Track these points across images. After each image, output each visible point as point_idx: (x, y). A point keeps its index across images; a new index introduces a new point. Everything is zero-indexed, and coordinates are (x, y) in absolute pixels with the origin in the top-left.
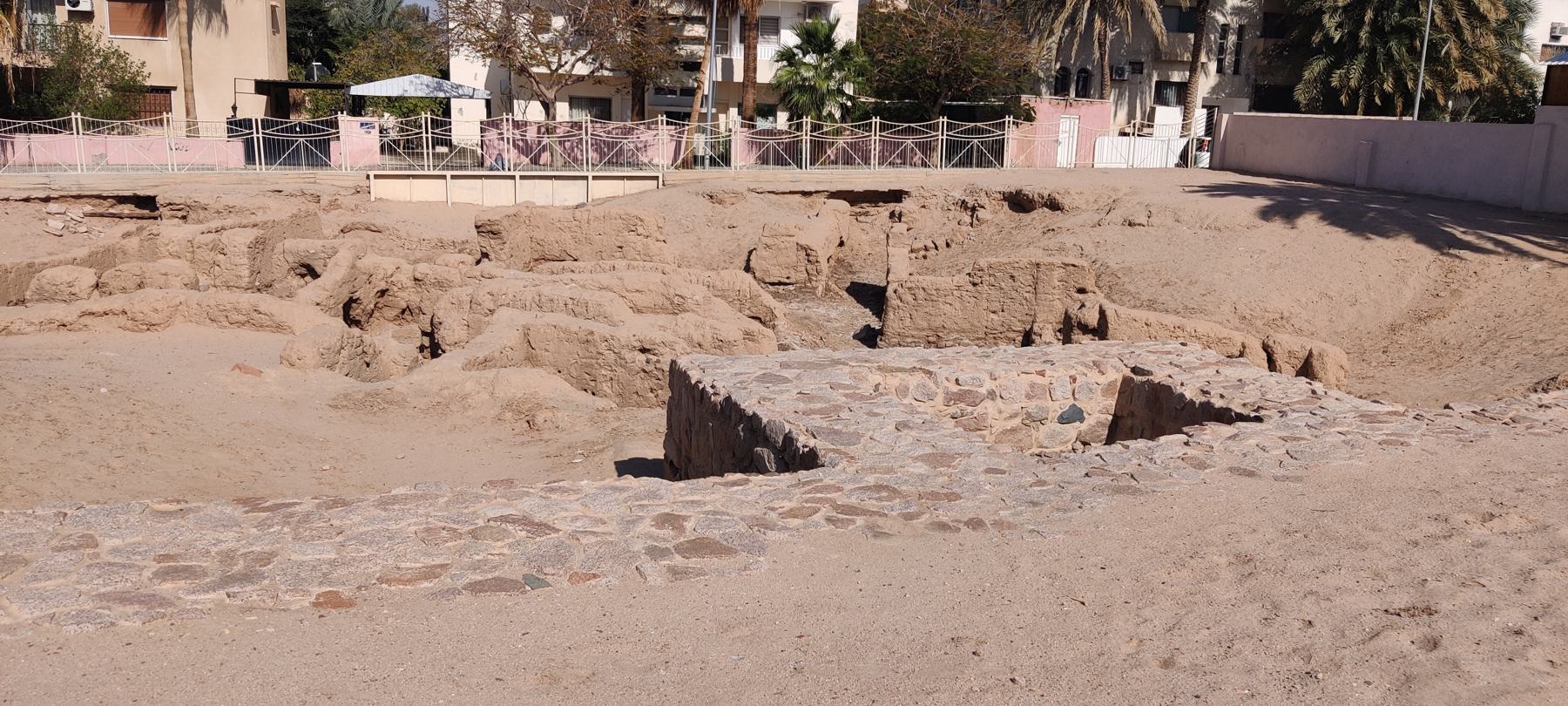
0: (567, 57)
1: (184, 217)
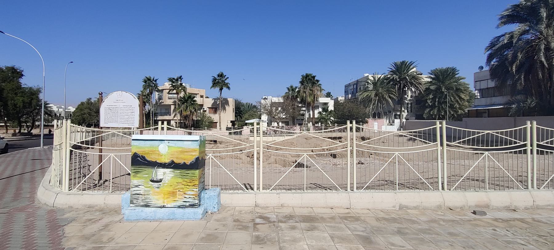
0: (281, 115)
1: (221, 144)
